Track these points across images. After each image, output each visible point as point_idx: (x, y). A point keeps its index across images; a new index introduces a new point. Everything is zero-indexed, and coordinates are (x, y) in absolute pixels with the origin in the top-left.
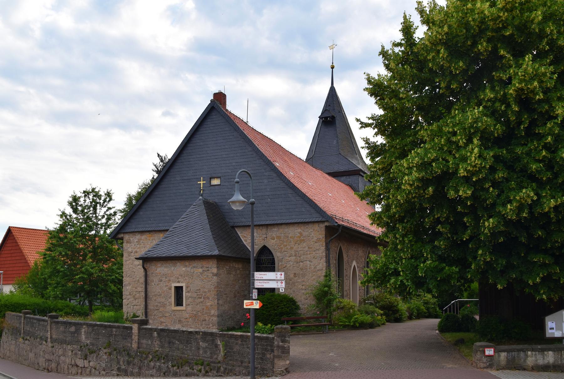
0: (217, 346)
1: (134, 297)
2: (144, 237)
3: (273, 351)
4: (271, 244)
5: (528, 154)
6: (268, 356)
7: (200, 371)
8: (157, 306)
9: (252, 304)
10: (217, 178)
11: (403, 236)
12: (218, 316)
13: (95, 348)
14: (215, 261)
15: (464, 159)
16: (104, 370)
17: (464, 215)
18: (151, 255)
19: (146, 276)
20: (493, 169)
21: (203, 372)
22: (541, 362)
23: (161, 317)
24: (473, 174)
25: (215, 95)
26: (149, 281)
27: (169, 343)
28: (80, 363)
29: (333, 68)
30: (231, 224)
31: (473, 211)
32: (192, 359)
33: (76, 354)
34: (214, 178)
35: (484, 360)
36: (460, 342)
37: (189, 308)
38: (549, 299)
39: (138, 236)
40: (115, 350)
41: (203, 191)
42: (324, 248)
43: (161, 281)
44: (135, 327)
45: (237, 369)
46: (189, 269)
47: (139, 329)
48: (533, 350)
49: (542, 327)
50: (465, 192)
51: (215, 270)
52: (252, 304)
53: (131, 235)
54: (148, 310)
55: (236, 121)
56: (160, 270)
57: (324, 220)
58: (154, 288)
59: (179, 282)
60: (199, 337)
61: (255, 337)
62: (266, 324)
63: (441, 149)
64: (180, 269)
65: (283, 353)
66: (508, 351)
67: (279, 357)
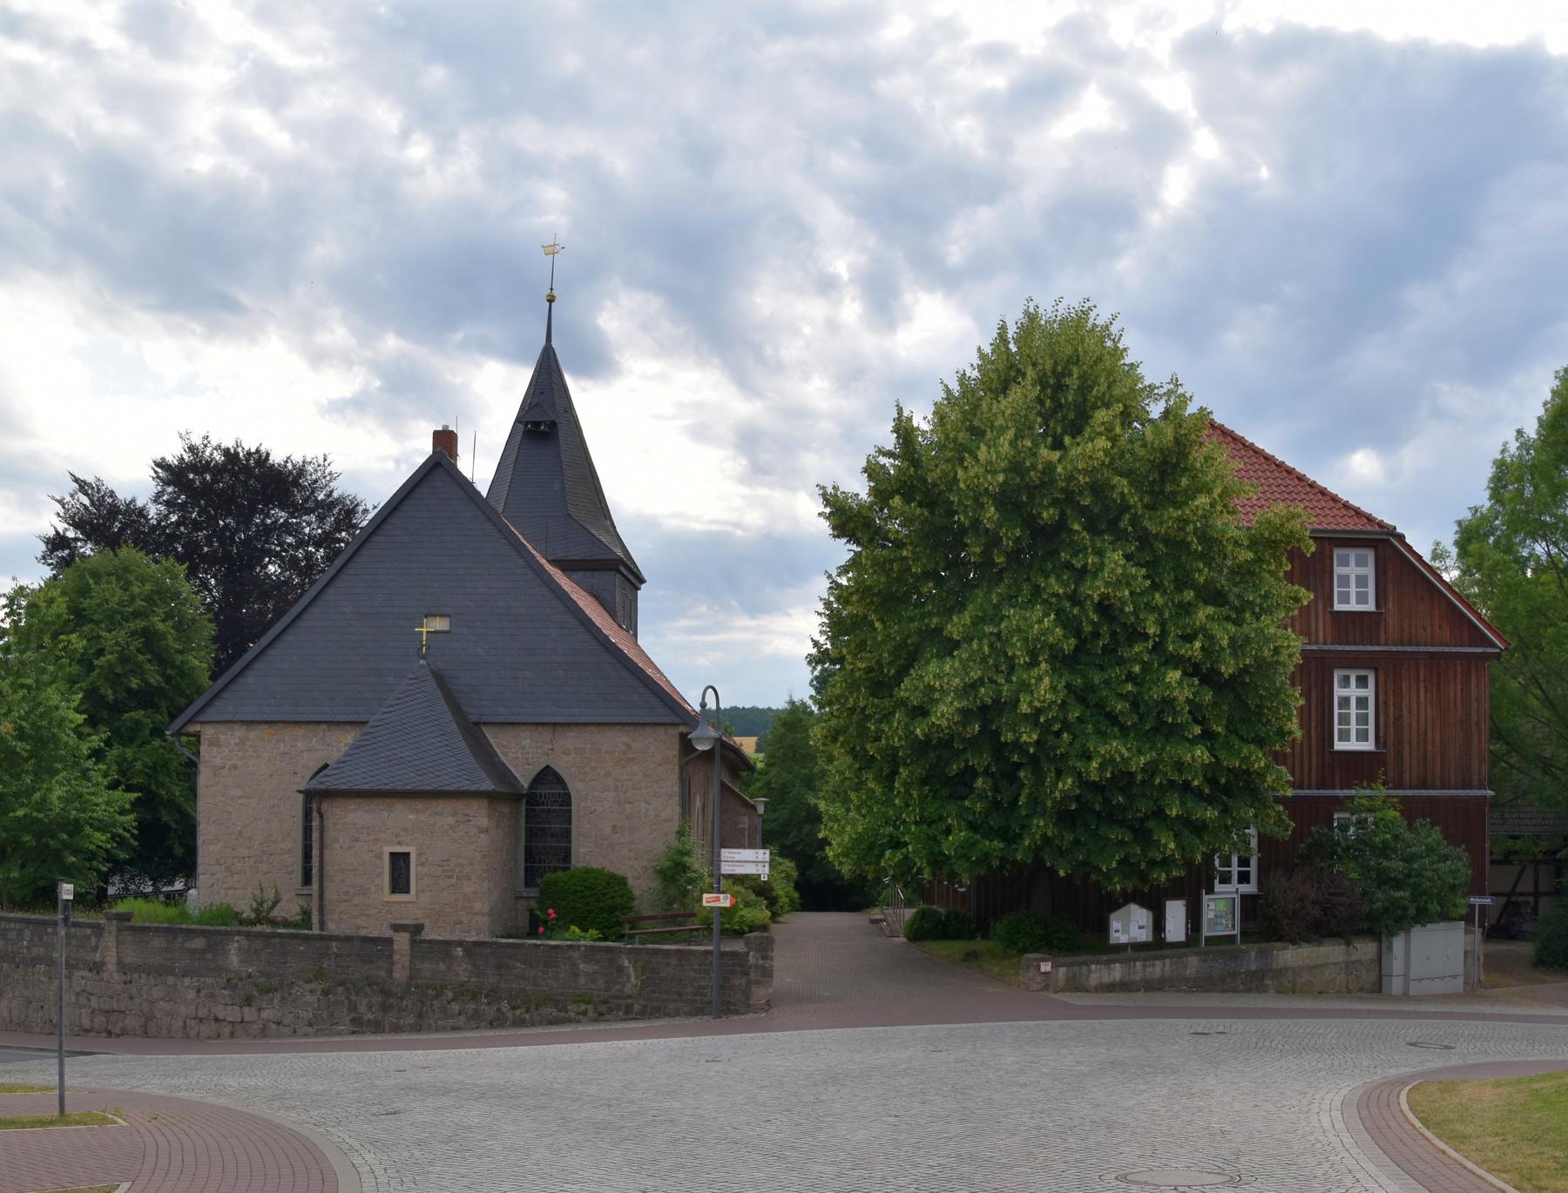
0: (620, 969)
1: (228, 869)
2: (255, 733)
3: (746, 973)
4: (562, 765)
5: (1107, 682)
6: (737, 982)
7: (585, 1013)
8: (347, 893)
9: (718, 899)
10: (442, 616)
12: (490, 914)
13: (275, 982)
14: (484, 803)
15: (1025, 687)
16: (311, 1025)
17: (1019, 766)
18: (329, 782)
21: (591, 1013)
22: (1106, 979)
23: (356, 917)
25: (436, 434)
26: (327, 840)
27: (499, 967)
28: (232, 1013)
29: (551, 300)
30: (473, 718)
32: (562, 994)
33: (212, 995)
34: (434, 615)
35: (1039, 978)
36: (971, 957)
39: (240, 732)
40: (341, 984)
41: (428, 647)
42: (676, 776)
43: (357, 840)
44: (402, 941)
45: (672, 1006)
47: (413, 942)
48: (1098, 963)
49: (1103, 928)
50: (1029, 736)
52: (718, 899)
53: (222, 728)
54: (326, 902)
56: (346, 820)
57: (677, 720)
59: (399, 843)
60: (576, 954)
61: (723, 955)
62: (585, 930)
64: (403, 815)
65: (764, 976)
67: (758, 982)
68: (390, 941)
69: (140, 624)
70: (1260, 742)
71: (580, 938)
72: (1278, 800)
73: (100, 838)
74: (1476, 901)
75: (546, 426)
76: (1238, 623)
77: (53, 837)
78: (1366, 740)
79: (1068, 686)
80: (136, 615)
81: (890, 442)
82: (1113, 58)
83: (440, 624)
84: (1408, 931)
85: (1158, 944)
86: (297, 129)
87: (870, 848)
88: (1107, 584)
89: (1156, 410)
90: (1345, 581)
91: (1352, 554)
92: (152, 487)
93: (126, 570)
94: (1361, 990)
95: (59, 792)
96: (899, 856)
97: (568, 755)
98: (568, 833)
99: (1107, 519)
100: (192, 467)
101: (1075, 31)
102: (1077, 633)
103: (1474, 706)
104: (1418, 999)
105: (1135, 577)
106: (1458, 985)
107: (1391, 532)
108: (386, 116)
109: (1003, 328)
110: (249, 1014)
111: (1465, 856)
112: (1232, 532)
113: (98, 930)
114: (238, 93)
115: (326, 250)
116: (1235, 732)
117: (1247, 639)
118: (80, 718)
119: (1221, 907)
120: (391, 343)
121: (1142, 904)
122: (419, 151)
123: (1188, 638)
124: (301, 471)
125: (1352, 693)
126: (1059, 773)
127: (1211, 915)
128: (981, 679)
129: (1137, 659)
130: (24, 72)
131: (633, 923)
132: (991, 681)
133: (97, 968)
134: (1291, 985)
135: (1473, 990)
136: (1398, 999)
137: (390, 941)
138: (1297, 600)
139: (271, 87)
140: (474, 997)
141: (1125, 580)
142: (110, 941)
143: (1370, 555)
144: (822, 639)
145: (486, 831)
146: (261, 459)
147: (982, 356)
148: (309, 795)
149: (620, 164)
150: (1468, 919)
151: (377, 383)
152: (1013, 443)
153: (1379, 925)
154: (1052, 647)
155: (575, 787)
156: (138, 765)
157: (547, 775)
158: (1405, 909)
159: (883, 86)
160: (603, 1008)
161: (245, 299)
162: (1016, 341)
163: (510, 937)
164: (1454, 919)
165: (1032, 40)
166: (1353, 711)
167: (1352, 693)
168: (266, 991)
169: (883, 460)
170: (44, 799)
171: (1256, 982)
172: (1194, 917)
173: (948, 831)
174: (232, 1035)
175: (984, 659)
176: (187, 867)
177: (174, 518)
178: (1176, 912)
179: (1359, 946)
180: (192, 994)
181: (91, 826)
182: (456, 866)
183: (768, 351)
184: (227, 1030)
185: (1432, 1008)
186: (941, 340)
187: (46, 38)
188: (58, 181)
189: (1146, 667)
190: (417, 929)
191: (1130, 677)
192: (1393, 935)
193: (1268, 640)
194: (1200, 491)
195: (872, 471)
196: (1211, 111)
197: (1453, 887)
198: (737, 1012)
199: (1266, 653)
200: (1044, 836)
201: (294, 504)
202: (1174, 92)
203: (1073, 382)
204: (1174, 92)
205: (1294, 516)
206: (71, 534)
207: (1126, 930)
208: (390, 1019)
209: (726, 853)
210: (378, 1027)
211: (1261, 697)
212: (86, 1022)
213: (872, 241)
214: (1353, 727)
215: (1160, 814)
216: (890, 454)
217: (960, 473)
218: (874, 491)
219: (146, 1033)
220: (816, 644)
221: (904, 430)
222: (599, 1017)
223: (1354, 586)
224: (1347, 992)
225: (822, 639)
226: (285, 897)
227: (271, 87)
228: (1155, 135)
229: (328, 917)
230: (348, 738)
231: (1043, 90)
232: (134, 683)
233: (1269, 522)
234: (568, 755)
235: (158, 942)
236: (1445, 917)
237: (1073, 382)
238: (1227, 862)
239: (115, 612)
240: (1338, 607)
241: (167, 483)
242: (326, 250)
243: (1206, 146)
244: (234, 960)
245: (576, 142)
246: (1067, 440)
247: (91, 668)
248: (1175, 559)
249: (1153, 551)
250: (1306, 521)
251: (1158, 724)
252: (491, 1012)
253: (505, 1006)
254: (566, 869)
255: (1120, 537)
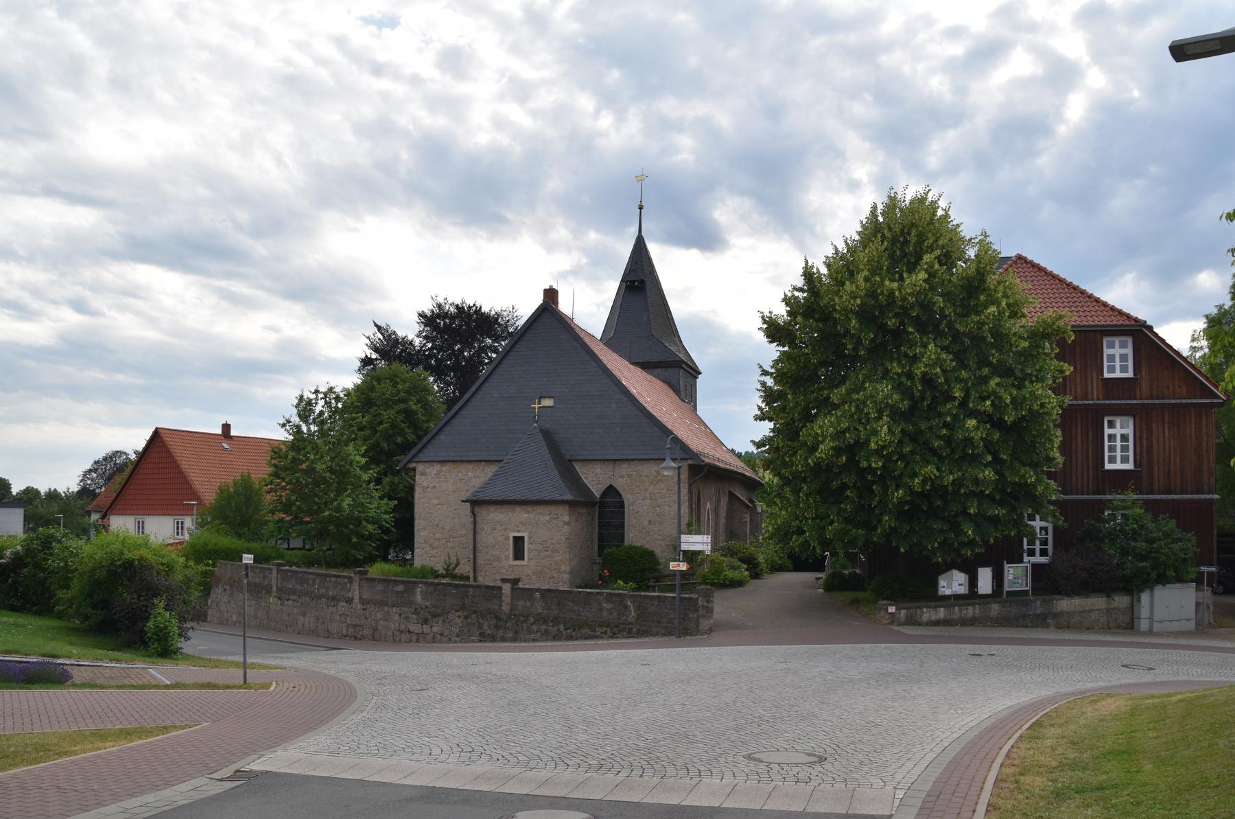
0: (626, 607)
3: (697, 611)
4: (620, 484)
5: (931, 428)
7: (605, 633)
11: (808, 495)
12: (571, 573)
13: (439, 611)
14: (567, 508)
15: (875, 432)
18: (480, 497)
19: (475, 523)
20: (900, 442)
21: (609, 633)
22: (934, 618)
24: (883, 447)
25: (545, 291)
27: (559, 604)
28: (416, 628)
29: (641, 208)
30: (568, 457)
31: (882, 479)
33: (407, 618)
36: (855, 602)
37: (533, 563)
38: (944, 561)
39: (437, 467)
40: (475, 612)
44: (507, 588)
46: (532, 516)
47: (512, 589)
49: (935, 585)
50: (877, 464)
51: (566, 518)
55: (577, 330)
56: (492, 516)
58: (485, 538)
61: (682, 599)
63: (852, 416)
66: (907, 609)
67: (704, 617)
68: (500, 588)
69: (403, 406)
70: (1035, 465)
71: (626, 589)
72: (1050, 502)
73: (370, 527)
74: (1204, 569)
75: (639, 282)
76: (1019, 388)
77: (346, 527)
78: (1128, 462)
79: (903, 431)
80: (401, 401)
81: (800, 282)
82: (1032, 27)
83: (547, 402)
84: (1152, 589)
85: (973, 595)
86: (534, 114)
87: (787, 534)
88: (926, 366)
89: (971, 253)
90: (1112, 358)
91: (1117, 341)
92: (417, 328)
93: (396, 376)
94: (1118, 627)
95: (348, 501)
96: (801, 539)
97: (623, 478)
98: (622, 526)
99: (928, 323)
100: (438, 316)
101: (1005, 14)
102: (912, 397)
103: (1205, 438)
104: (1158, 634)
105: (945, 360)
106: (1191, 625)
107: (1143, 324)
108: (585, 102)
109: (874, 208)
110: (426, 629)
111: (1194, 539)
112: (1016, 329)
113: (350, 579)
114: (502, 97)
115: (554, 184)
116: (1017, 459)
117: (1024, 398)
118: (364, 460)
119: (1016, 576)
120: (592, 236)
121: (961, 570)
122: (606, 121)
123: (983, 399)
124: (498, 315)
125: (1120, 430)
126: (897, 488)
127: (1011, 577)
128: (849, 428)
129: (949, 413)
130: (385, 96)
131: (657, 579)
132: (855, 429)
133: (349, 601)
134: (1066, 623)
135: (1203, 628)
136: (1142, 634)
137: (500, 588)
138: (1061, 371)
139: (520, 91)
140: (545, 622)
141: (938, 362)
142: (356, 586)
143: (1130, 341)
144: (763, 406)
145: (568, 524)
146: (478, 311)
147: (863, 226)
148: (476, 503)
149: (724, 120)
150: (1199, 581)
151: (585, 261)
152: (867, 279)
153: (1134, 584)
154: (892, 407)
155: (627, 497)
156: (401, 486)
157: (611, 491)
158: (1149, 574)
159: (884, 59)
160: (616, 630)
161: (510, 216)
162: (882, 214)
163: (587, 587)
164: (1186, 582)
165: (979, 24)
166: (1118, 443)
167: (1120, 430)
168: (435, 616)
169: (797, 294)
170: (339, 505)
171: (1041, 621)
172: (998, 578)
173: (832, 522)
174: (417, 641)
175: (852, 416)
176: (410, 546)
177: (430, 345)
178: (985, 579)
179: (1116, 598)
180: (397, 617)
181: (367, 521)
182: (546, 545)
183: (818, 229)
184: (415, 638)
185: (1163, 641)
186: (839, 216)
187: (397, 76)
188: (404, 155)
189: (955, 417)
190: (515, 582)
191: (946, 425)
192: (1141, 591)
193: (1037, 398)
194: (993, 303)
195: (787, 300)
196: (1098, 55)
197: (1184, 560)
198: (691, 635)
199: (1035, 407)
200: (890, 526)
201: (495, 335)
202: (1072, 45)
203: (913, 238)
204: (1072, 45)
205: (1060, 317)
206: (374, 356)
207: (950, 586)
208: (500, 633)
209: (684, 538)
210: (493, 639)
211: (1035, 436)
212: (344, 632)
213: (881, 156)
214: (1119, 454)
215: (964, 512)
216: (800, 290)
217: (837, 300)
218: (789, 313)
219: (374, 639)
220: (760, 408)
221: (808, 274)
222: (614, 636)
223: (1118, 360)
224: (1107, 628)
225: (763, 406)
226: (462, 562)
227: (520, 91)
228: (1061, 75)
229: (478, 574)
230: (491, 470)
231: (987, 53)
232: (399, 440)
233: (1044, 322)
234: (623, 478)
235: (380, 587)
236: (1179, 579)
237: (913, 238)
238: (1031, 543)
239: (389, 400)
240: (1107, 375)
241: (426, 325)
242: (554, 184)
243: (1096, 79)
244: (419, 598)
245: (698, 109)
246: (905, 275)
247: (376, 432)
248: (972, 349)
249: (963, 343)
250: (1070, 318)
251: (962, 454)
252: (554, 630)
253: (562, 627)
254: (618, 546)
255: (939, 334)
